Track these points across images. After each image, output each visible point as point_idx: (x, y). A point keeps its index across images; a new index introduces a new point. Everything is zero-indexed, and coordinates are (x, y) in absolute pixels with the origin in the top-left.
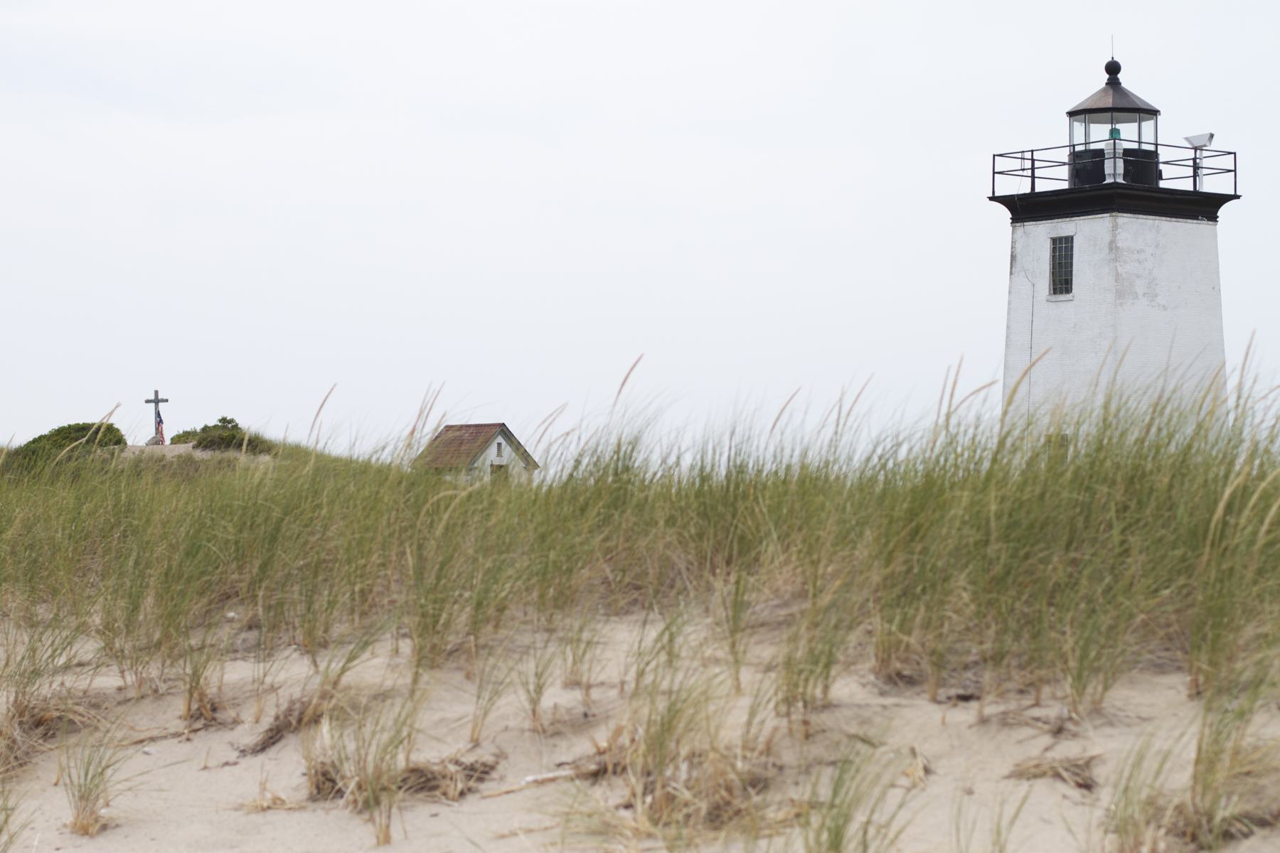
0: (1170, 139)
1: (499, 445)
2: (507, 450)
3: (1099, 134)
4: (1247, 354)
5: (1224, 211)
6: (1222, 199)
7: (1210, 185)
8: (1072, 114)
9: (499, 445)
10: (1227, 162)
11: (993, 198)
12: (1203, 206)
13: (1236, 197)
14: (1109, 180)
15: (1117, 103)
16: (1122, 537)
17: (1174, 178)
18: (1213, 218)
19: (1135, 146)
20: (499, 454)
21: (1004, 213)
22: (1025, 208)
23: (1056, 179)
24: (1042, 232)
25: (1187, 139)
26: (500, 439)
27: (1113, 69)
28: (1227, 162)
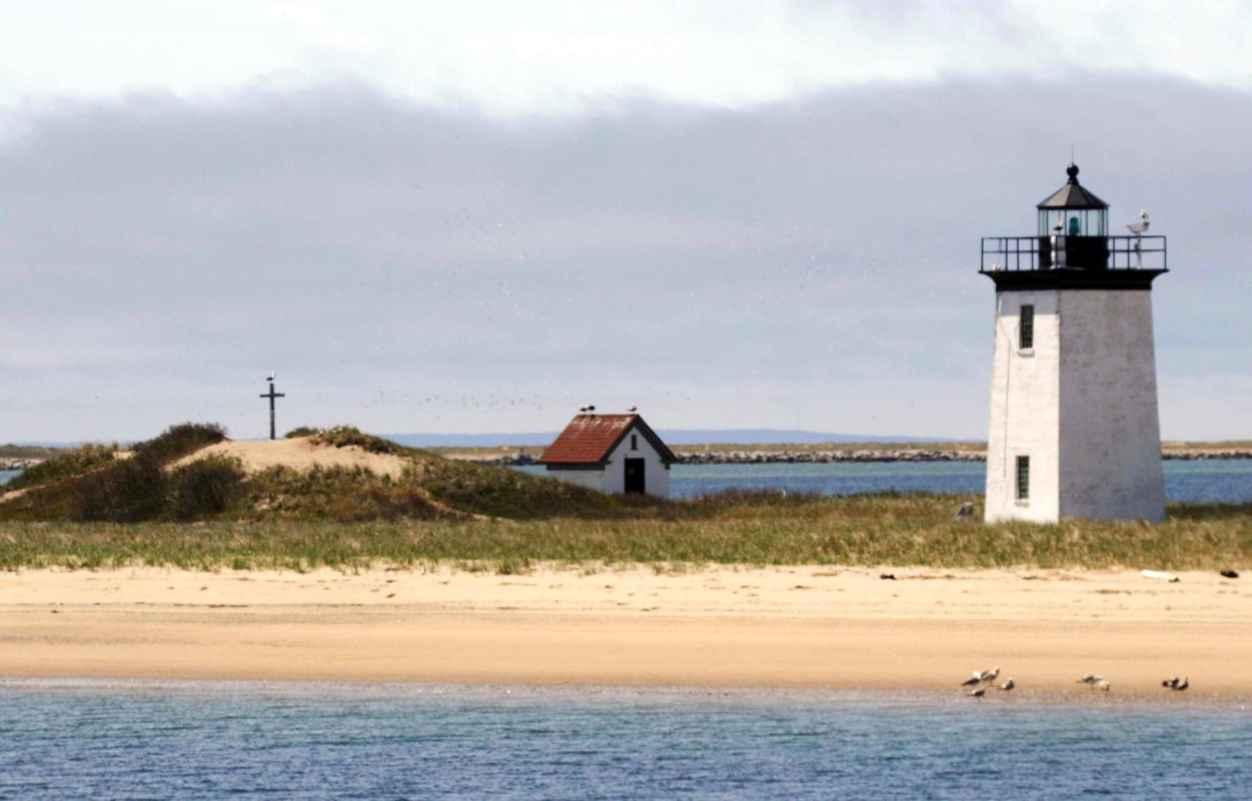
0: (1117, 223)
1: (634, 439)
2: (642, 441)
3: (1058, 220)
4: (273, 423)
5: (1157, 282)
6: (1153, 273)
7: (1148, 262)
8: (1042, 208)
9: (634, 439)
10: (1158, 244)
11: (982, 272)
12: (1141, 280)
13: (1165, 270)
14: (1053, 267)
15: (1082, 200)
16: (830, 459)
17: (1118, 262)
18: (1147, 287)
19: (1036, 256)
20: (634, 447)
21: (990, 284)
22: (1006, 281)
23: (1028, 263)
24: (1017, 298)
25: (1129, 227)
26: (634, 431)
27: (1073, 171)
28: (1158, 244)
